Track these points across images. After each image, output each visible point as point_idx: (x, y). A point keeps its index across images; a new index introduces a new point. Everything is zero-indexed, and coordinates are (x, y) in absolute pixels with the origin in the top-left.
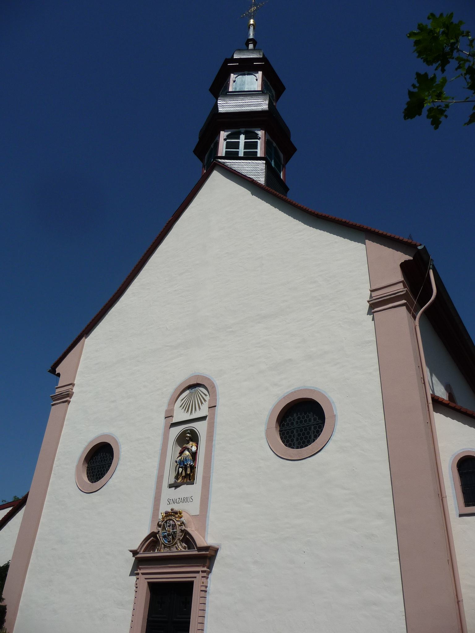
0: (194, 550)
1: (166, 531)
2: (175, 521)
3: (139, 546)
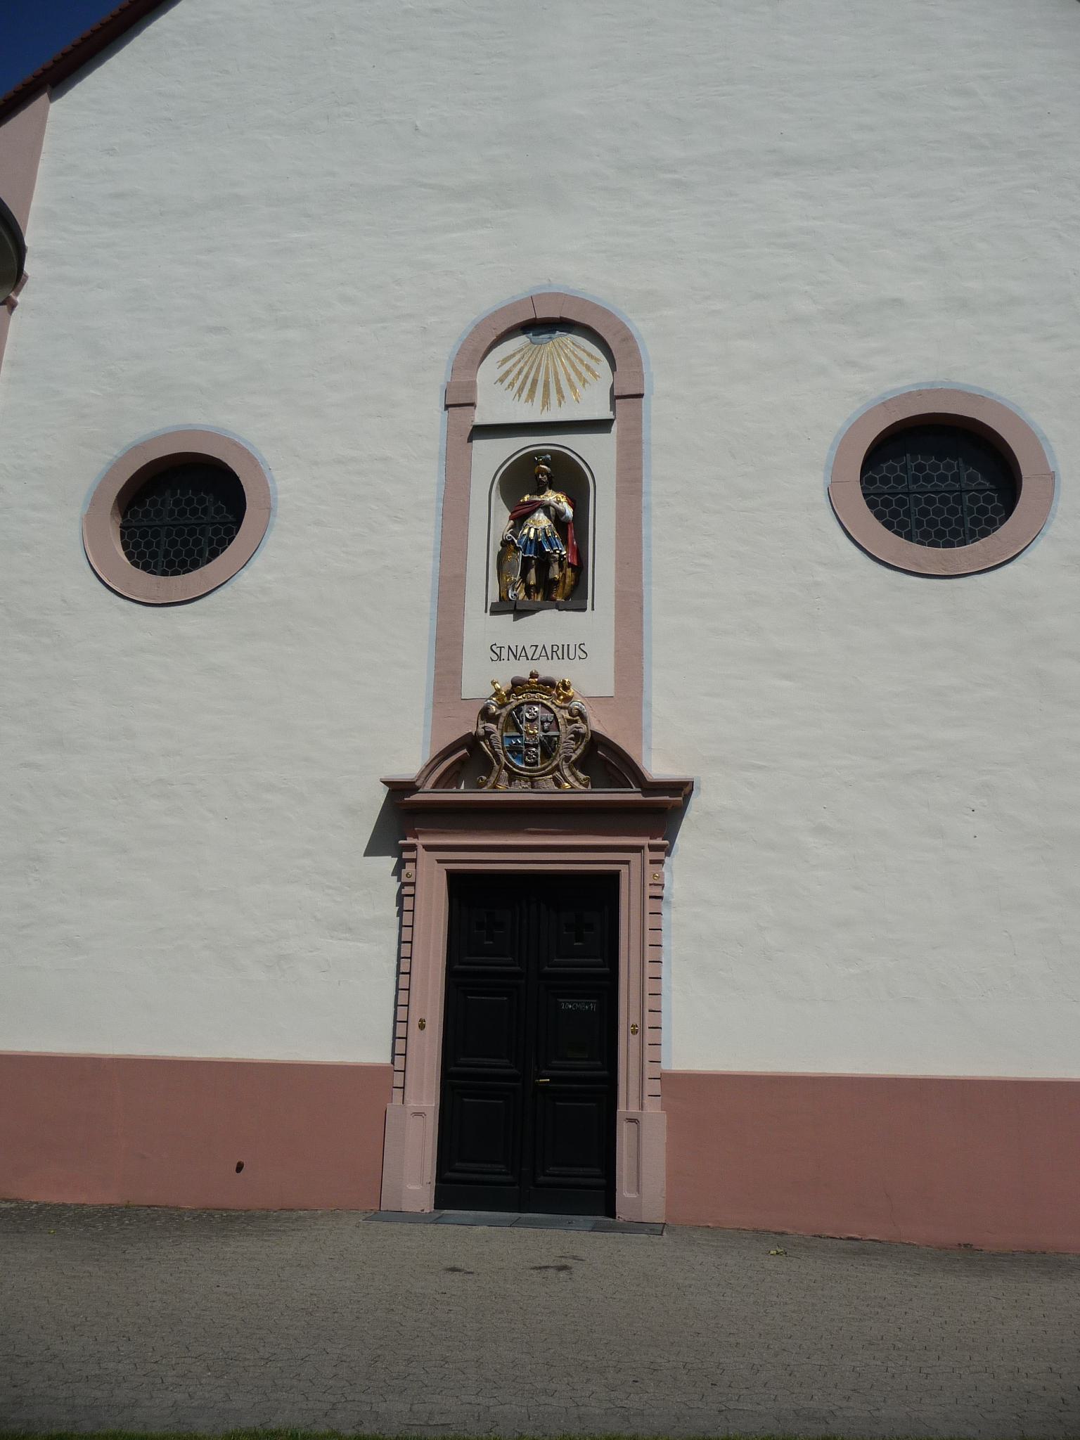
0: (631, 790)
1: (518, 734)
2: (553, 707)
3: (423, 772)
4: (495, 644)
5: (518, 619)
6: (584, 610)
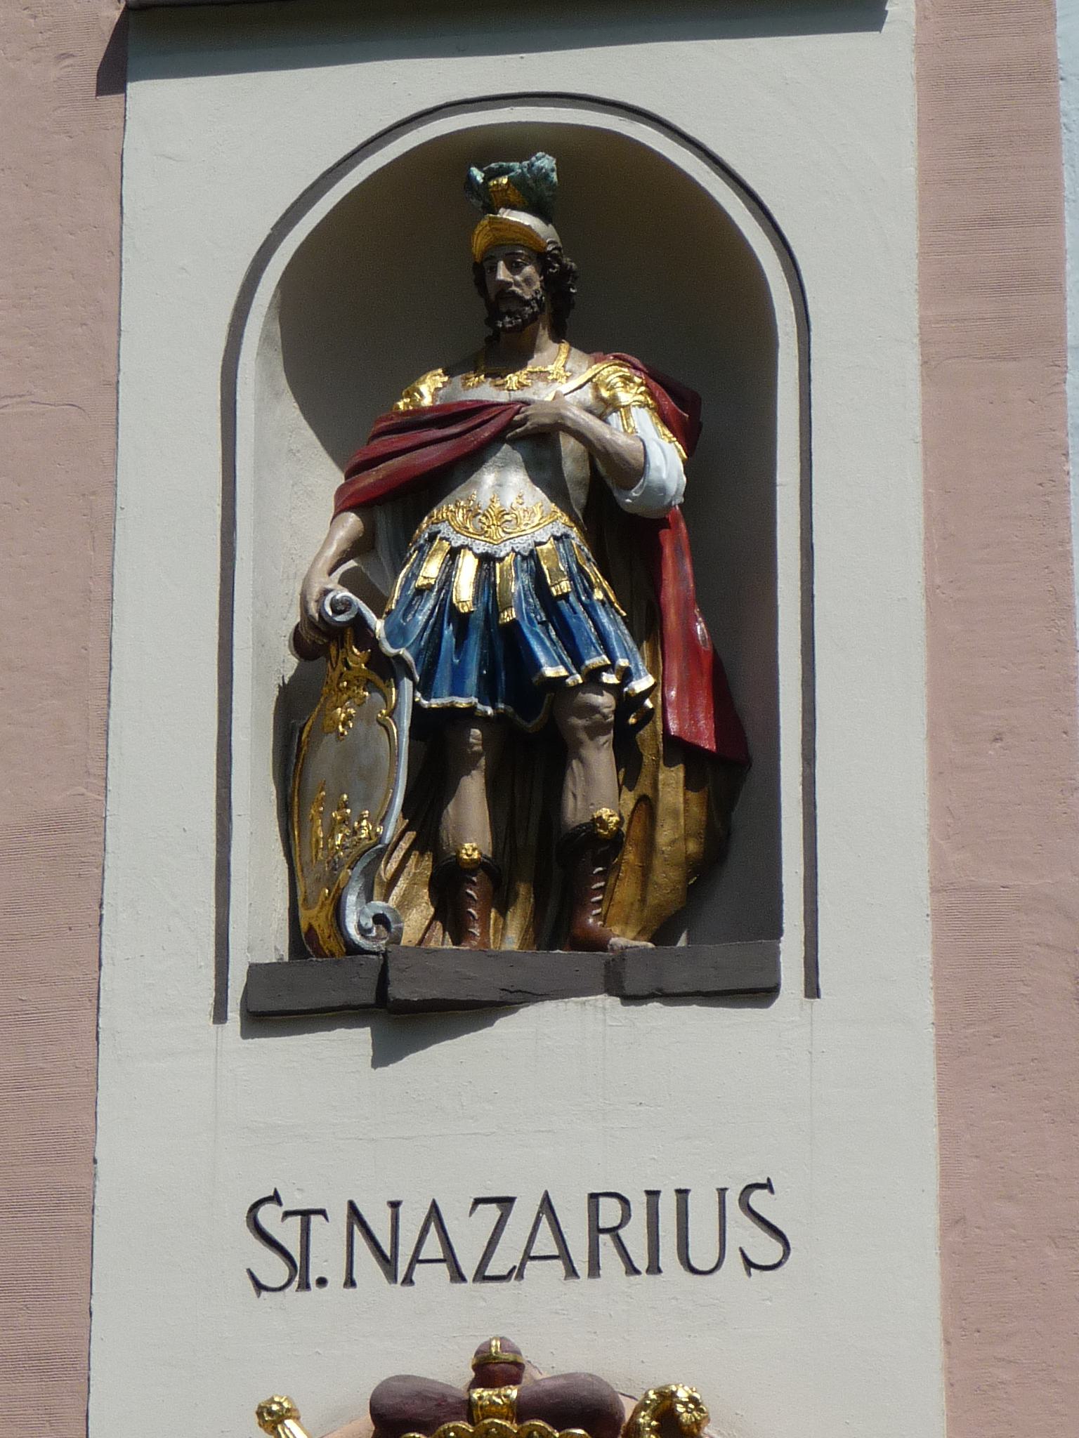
4: (275, 1198)
5: (385, 1064)
6: (764, 994)
